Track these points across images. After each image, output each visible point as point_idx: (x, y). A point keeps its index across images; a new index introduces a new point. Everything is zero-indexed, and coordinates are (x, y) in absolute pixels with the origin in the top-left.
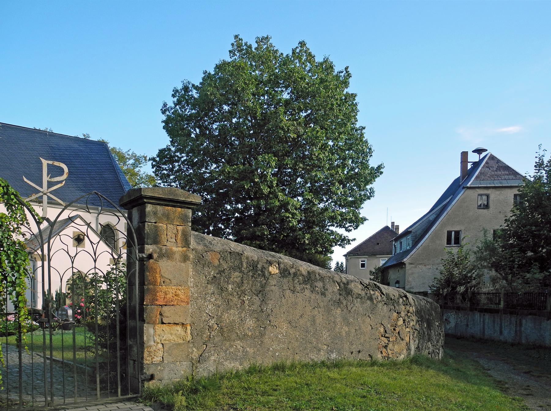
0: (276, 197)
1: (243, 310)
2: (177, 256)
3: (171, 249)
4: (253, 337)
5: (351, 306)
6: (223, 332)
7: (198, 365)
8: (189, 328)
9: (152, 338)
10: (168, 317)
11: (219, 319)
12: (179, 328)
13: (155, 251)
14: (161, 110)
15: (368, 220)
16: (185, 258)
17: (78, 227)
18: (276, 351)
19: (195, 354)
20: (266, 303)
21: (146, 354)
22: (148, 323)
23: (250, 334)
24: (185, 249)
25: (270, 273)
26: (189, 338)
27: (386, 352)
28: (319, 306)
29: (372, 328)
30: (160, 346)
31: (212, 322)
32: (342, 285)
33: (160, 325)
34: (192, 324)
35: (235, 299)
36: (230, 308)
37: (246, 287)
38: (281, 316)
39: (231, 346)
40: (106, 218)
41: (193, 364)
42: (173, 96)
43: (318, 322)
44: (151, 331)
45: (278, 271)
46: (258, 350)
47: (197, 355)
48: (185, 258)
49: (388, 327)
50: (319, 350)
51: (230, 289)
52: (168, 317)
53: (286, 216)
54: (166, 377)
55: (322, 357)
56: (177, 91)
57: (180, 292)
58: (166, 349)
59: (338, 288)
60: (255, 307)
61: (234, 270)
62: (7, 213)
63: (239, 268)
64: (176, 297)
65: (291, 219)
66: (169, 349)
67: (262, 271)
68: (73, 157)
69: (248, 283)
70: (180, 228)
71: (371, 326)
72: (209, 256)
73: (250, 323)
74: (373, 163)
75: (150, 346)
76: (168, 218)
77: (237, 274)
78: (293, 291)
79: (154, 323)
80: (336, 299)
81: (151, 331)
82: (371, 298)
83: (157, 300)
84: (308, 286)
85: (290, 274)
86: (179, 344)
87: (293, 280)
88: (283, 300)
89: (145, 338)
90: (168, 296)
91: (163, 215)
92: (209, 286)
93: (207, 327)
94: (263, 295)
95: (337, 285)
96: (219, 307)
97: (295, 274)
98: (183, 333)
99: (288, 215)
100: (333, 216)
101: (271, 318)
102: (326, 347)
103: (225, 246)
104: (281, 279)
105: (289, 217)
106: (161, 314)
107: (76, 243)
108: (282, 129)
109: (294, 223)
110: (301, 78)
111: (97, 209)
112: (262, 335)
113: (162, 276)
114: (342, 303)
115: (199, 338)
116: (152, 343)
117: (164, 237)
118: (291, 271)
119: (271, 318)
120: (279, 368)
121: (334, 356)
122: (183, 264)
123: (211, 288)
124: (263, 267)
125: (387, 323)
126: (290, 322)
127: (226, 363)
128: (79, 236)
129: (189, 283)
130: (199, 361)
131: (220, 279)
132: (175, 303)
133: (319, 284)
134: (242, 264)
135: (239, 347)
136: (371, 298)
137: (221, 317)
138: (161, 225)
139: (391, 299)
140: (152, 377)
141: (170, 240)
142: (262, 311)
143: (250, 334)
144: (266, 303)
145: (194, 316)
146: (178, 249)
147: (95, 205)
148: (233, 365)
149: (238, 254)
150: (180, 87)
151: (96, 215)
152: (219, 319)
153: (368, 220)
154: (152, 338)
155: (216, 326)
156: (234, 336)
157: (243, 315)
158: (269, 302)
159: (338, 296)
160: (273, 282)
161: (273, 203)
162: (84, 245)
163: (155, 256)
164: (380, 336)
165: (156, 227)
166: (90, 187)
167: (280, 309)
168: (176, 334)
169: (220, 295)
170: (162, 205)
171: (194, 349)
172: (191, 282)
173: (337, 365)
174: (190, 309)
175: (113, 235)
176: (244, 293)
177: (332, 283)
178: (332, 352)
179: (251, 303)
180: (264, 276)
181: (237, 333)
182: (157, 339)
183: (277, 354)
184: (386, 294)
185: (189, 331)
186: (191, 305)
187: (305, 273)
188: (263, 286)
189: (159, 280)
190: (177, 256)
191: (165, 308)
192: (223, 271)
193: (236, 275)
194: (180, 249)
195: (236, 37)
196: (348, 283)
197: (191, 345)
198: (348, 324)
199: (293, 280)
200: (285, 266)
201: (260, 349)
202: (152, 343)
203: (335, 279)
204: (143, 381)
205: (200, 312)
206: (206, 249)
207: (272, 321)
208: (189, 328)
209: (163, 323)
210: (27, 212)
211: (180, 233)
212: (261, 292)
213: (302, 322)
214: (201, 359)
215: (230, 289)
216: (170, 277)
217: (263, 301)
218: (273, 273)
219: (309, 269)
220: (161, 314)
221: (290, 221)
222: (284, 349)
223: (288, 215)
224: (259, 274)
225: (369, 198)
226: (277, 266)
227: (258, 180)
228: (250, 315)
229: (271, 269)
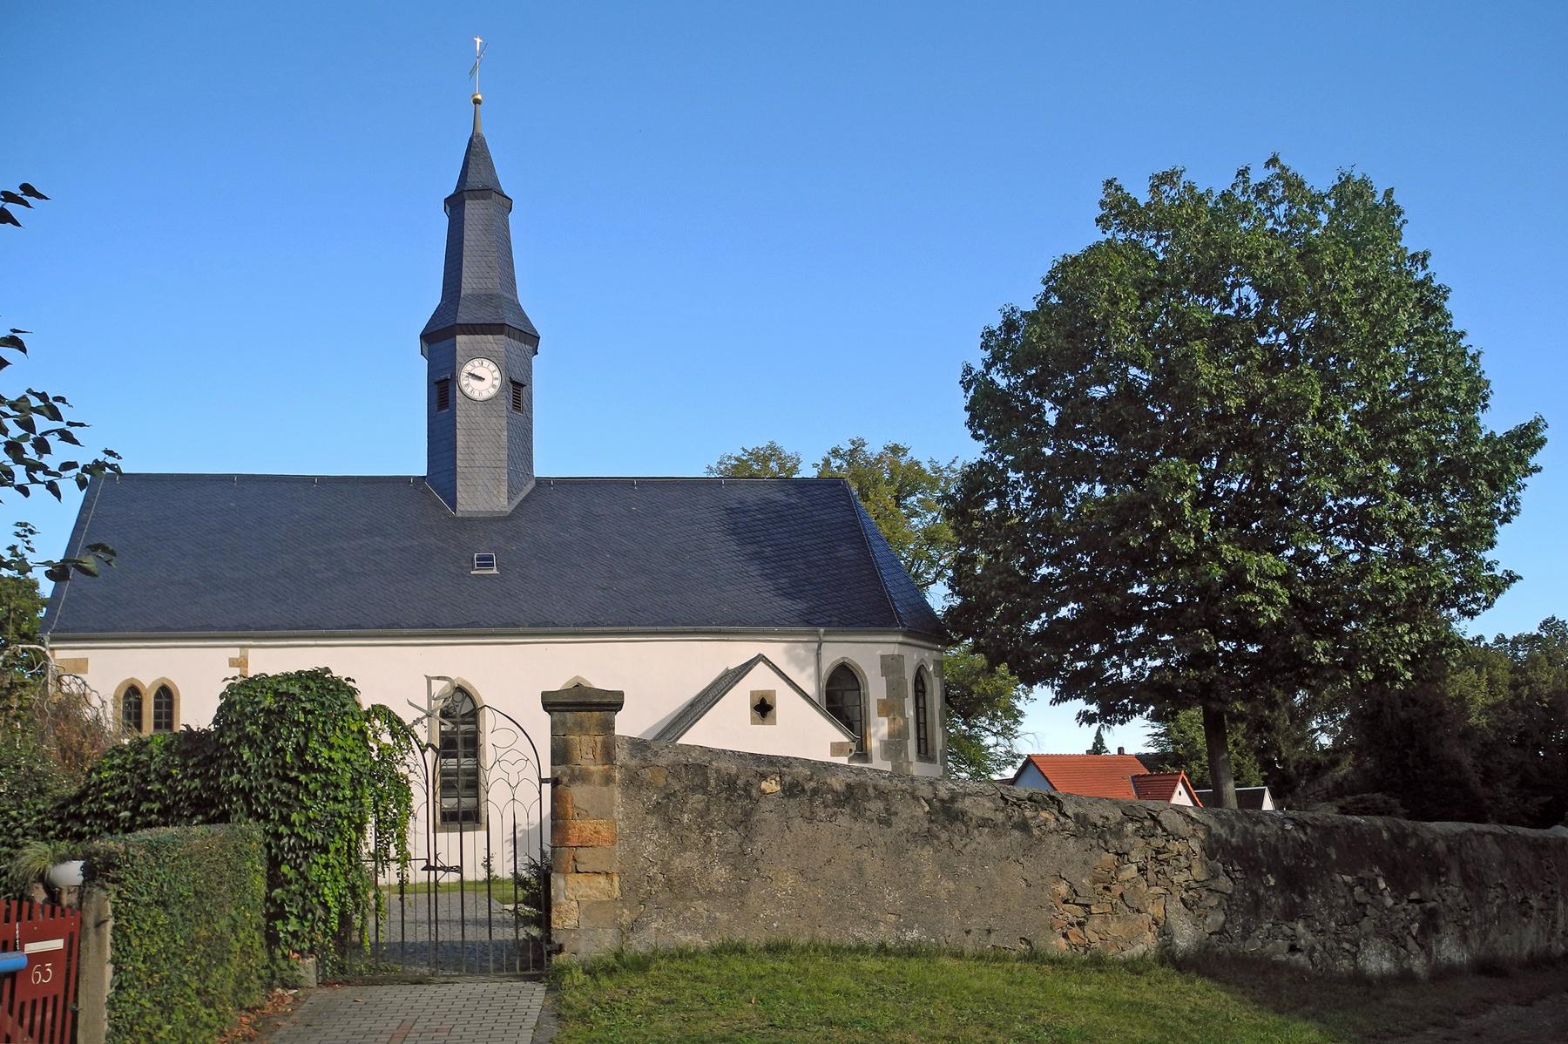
0: (1216, 555)
1: (709, 852)
2: (596, 778)
3: (587, 770)
4: (726, 895)
5: (963, 842)
6: (673, 885)
7: (630, 934)
8: (616, 879)
9: (562, 893)
10: (584, 863)
11: (666, 867)
12: (602, 880)
13: (564, 774)
14: (961, 382)
15: (1521, 578)
16: (608, 780)
17: (760, 679)
18: (775, 919)
19: (627, 917)
20: (751, 841)
21: (554, 916)
22: (557, 872)
23: (720, 889)
24: (606, 767)
25: (763, 792)
26: (617, 894)
27: (1082, 935)
28: (871, 844)
29: (1029, 886)
30: (574, 904)
31: (653, 871)
32: (937, 804)
33: (573, 875)
34: (621, 873)
35: (694, 836)
36: (685, 850)
37: (714, 815)
38: (781, 862)
39: (688, 908)
40: (838, 650)
41: (623, 933)
42: (985, 346)
43: (869, 871)
44: (561, 883)
45: (779, 788)
46: (736, 917)
47: (629, 920)
48: (608, 780)
49: (1083, 884)
50: (876, 922)
51: (686, 820)
52: (584, 863)
53: (1244, 602)
54: (583, 950)
55: (884, 933)
56: (991, 333)
57: (601, 828)
58: (582, 908)
59: (927, 809)
60: (729, 847)
61: (694, 790)
62: (391, 743)
63: (703, 788)
64: (596, 835)
65: (1261, 608)
66: (587, 908)
67: (745, 790)
68: (773, 523)
69: (719, 811)
70: (599, 739)
71: (1026, 880)
72: (647, 774)
73: (720, 872)
74: (1496, 421)
75: (560, 904)
76: (581, 727)
77: (699, 796)
78: (810, 820)
79: (565, 873)
80: (920, 830)
81: (561, 883)
82: (1024, 826)
83: (568, 840)
84: (847, 810)
85: (803, 790)
86: (602, 903)
87: (811, 801)
88: (788, 835)
89: (553, 893)
90: (584, 834)
91: (574, 724)
92: (649, 817)
93: (646, 878)
94: (746, 827)
95: (925, 804)
96: (665, 848)
97: (815, 791)
98: (608, 887)
99: (1247, 598)
100: (1386, 584)
101: (761, 864)
102: (893, 917)
103: (681, 756)
104: (786, 800)
105: (1253, 603)
106: (575, 860)
107: (757, 715)
108: (1206, 393)
109: (1272, 615)
110: (1249, 257)
111: (817, 634)
112: (743, 892)
113: (575, 807)
114: (938, 838)
115: (632, 894)
116: (563, 900)
117: (576, 753)
118: (806, 787)
119: (761, 864)
120: (776, 949)
121: (913, 935)
122: (605, 789)
123: (653, 821)
124: (748, 784)
125: (1078, 875)
126: (802, 872)
127: (679, 935)
128: (763, 701)
129: (615, 815)
130: (632, 929)
131: (667, 806)
132: (595, 844)
133: (876, 806)
134: (708, 783)
135: (701, 910)
136: (1024, 826)
137: (668, 863)
138: (572, 737)
139: (1095, 826)
140: (560, 949)
141: (585, 756)
142: (743, 853)
143: (720, 889)
144: (751, 841)
145: (624, 862)
146: (596, 768)
147: (812, 625)
148: (689, 937)
149: (700, 766)
150: (996, 322)
151: (816, 645)
152: (666, 867)
153: (1521, 578)
154: (562, 893)
155: (660, 877)
156: (691, 893)
157: (708, 860)
158: (758, 838)
159: (926, 825)
160: (765, 806)
161: (1208, 574)
162: (774, 717)
163: (565, 780)
164: (1058, 901)
165: (565, 741)
166: (803, 586)
167: (779, 850)
168: (597, 888)
169: (667, 829)
170: (572, 711)
171: (625, 910)
172: (618, 812)
173: (911, 952)
174: (618, 851)
175: (856, 686)
176: (710, 825)
177: (911, 801)
178: (912, 929)
179: (724, 841)
180: (749, 796)
181: (697, 888)
182: (569, 894)
183: (775, 925)
184: (1077, 816)
185: (616, 884)
186: (620, 845)
187: (839, 788)
188: (747, 814)
189: (571, 812)
190: (596, 778)
191: (581, 851)
192: (674, 794)
193: (696, 799)
194: (600, 767)
195: (1109, 183)
196: (953, 799)
197: (620, 905)
198: (954, 875)
199: (811, 801)
200: (793, 778)
201: (740, 914)
202: (563, 900)
203: (919, 793)
204: (549, 954)
205: (634, 856)
206: (643, 764)
207: (763, 870)
208: (616, 879)
209: (578, 872)
210: (412, 739)
211: (599, 745)
212: (745, 823)
213: (829, 872)
214: (635, 926)
215: (686, 820)
216: (587, 808)
217: (748, 838)
218: (768, 791)
219: (848, 780)
220: (575, 860)
221: (1259, 614)
222: (790, 916)
223: (1247, 598)
224: (740, 796)
225: (1506, 519)
226: (778, 779)
227: (1160, 523)
228: (721, 860)
229: (764, 785)
